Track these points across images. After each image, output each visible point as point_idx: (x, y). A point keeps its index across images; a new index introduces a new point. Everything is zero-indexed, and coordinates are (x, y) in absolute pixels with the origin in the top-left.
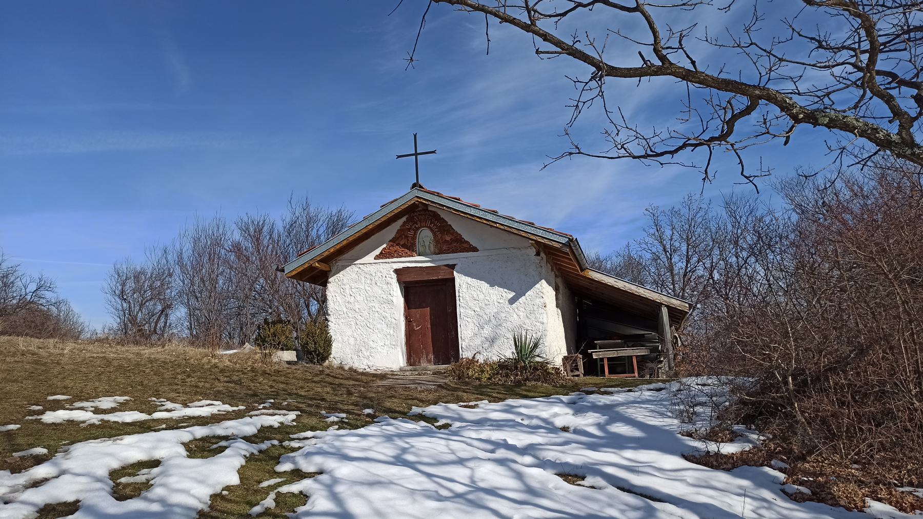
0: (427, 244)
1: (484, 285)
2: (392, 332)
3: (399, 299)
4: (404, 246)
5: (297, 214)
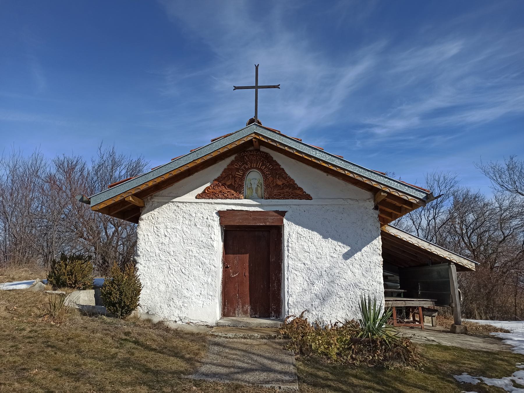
0: (254, 186)
1: (316, 236)
2: (210, 280)
3: (219, 245)
4: (230, 186)
5: (104, 158)
